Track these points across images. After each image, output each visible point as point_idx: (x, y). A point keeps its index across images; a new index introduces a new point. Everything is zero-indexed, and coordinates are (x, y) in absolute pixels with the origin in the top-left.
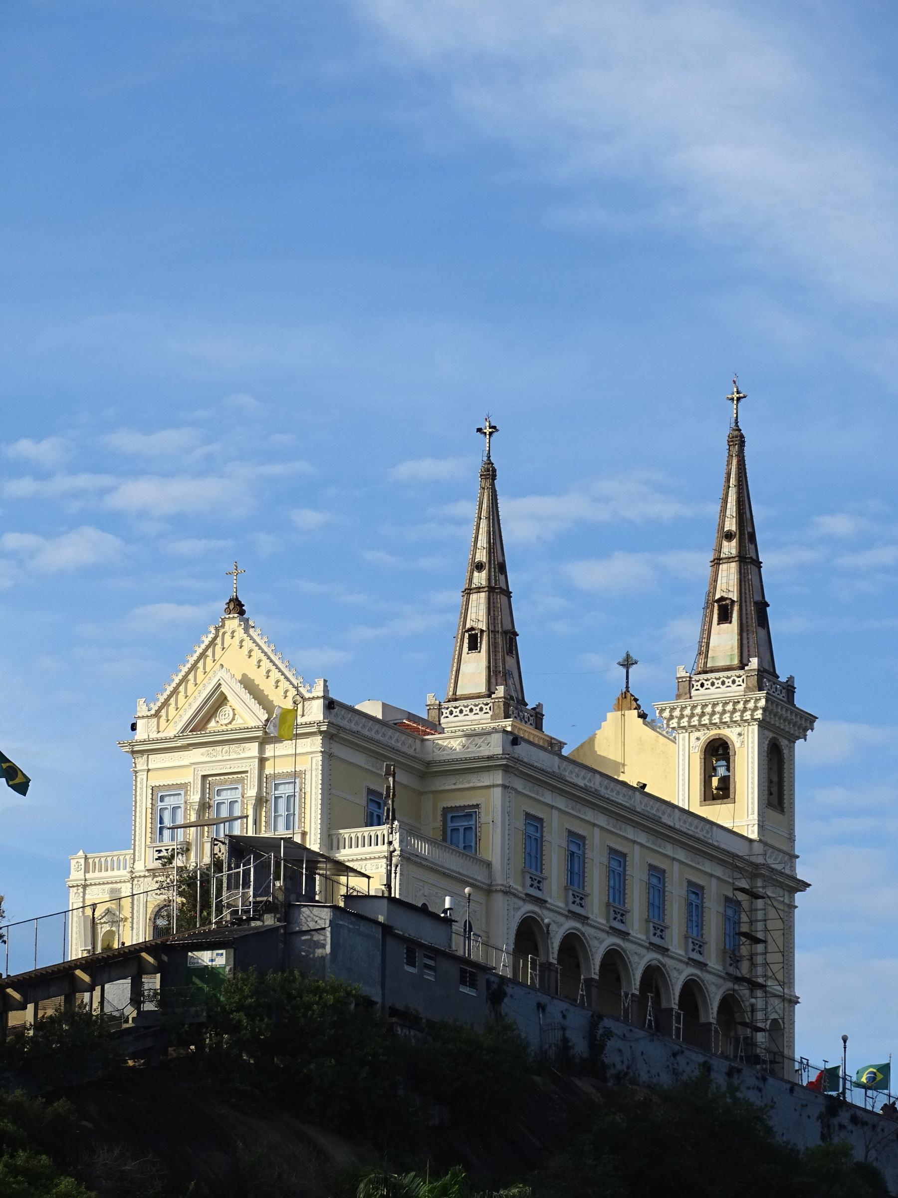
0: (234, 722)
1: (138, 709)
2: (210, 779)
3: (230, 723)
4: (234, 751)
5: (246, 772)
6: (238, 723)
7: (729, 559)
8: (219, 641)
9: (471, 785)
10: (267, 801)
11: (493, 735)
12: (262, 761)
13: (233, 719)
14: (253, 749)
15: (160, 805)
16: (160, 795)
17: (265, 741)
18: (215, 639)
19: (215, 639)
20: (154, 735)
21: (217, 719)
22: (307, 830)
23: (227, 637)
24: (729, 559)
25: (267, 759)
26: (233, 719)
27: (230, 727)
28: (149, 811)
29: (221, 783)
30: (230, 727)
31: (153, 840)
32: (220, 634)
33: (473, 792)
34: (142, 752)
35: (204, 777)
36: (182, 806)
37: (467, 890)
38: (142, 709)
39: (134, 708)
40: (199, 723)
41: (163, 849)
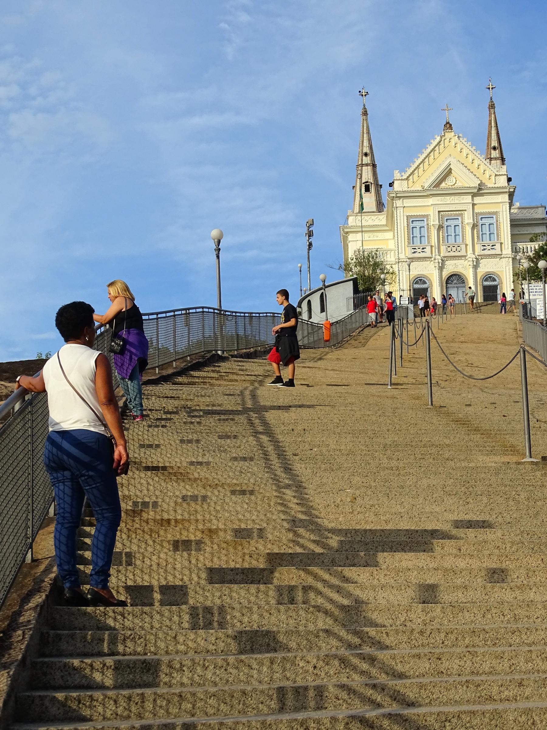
0: (456, 185)
1: (395, 175)
2: (442, 213)
3: (454, 185)
4: (456, 199)
5: (466, 210)
6: (459, 184)
7: (367, 165)
8: (442, 142)
9: (529, 232)
10: (477, 226)
11: (539, 208)
12: (474, 205)
13: (456, 183)
14: (468, 199)
15: (412, 225)
16: (411, 220)
17: (474, 195)
18: (440, 142)
19: (440, 142)
20: (406, 189)
21: (446, 182)
22: (503, 241)
23: (447, 141)
24: (367, 165)
25: (475, 204)
26: (456, 183)
27: (453, 187)
28: (406, 228)
29: (448, 215)
30: (453, 187)
31: (409, 243)
32: (443, 140)
33: (520, 236)
34: (400, 197)
35: (439, 212)
36: (426, 227)
37: (189, 358)
38: (397, 175)
39: (393, 175)
40: (437, 184)
41: (416, 248)
